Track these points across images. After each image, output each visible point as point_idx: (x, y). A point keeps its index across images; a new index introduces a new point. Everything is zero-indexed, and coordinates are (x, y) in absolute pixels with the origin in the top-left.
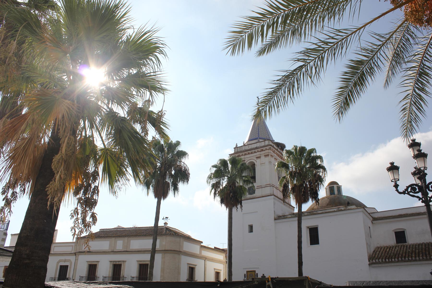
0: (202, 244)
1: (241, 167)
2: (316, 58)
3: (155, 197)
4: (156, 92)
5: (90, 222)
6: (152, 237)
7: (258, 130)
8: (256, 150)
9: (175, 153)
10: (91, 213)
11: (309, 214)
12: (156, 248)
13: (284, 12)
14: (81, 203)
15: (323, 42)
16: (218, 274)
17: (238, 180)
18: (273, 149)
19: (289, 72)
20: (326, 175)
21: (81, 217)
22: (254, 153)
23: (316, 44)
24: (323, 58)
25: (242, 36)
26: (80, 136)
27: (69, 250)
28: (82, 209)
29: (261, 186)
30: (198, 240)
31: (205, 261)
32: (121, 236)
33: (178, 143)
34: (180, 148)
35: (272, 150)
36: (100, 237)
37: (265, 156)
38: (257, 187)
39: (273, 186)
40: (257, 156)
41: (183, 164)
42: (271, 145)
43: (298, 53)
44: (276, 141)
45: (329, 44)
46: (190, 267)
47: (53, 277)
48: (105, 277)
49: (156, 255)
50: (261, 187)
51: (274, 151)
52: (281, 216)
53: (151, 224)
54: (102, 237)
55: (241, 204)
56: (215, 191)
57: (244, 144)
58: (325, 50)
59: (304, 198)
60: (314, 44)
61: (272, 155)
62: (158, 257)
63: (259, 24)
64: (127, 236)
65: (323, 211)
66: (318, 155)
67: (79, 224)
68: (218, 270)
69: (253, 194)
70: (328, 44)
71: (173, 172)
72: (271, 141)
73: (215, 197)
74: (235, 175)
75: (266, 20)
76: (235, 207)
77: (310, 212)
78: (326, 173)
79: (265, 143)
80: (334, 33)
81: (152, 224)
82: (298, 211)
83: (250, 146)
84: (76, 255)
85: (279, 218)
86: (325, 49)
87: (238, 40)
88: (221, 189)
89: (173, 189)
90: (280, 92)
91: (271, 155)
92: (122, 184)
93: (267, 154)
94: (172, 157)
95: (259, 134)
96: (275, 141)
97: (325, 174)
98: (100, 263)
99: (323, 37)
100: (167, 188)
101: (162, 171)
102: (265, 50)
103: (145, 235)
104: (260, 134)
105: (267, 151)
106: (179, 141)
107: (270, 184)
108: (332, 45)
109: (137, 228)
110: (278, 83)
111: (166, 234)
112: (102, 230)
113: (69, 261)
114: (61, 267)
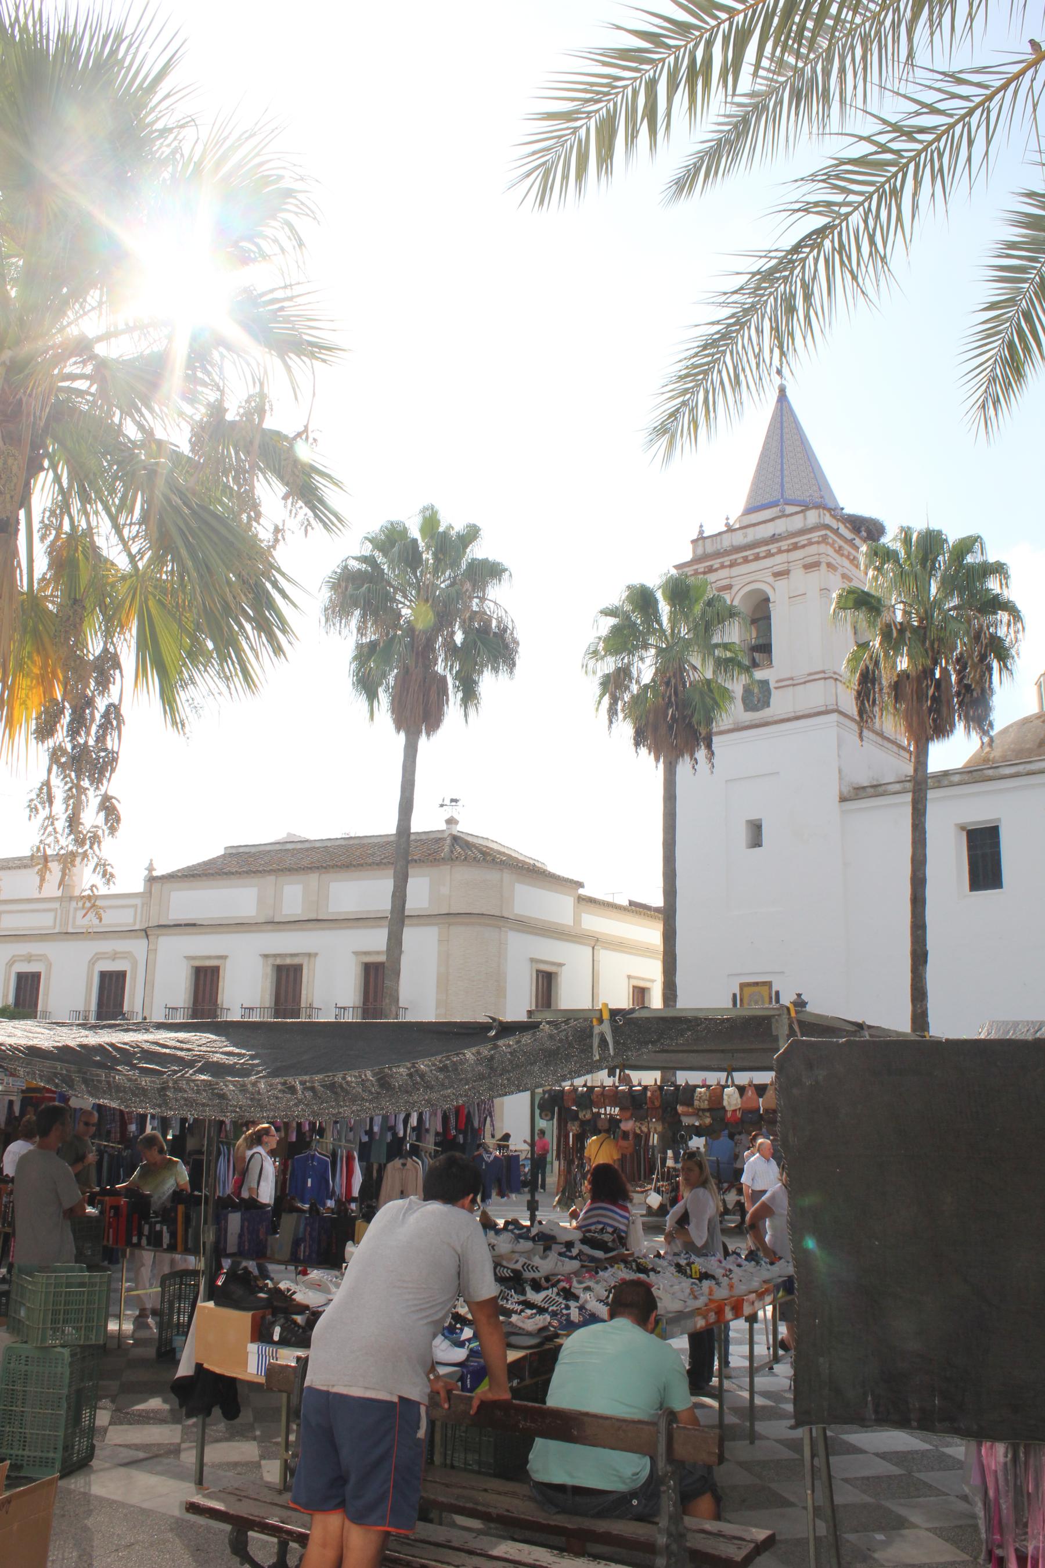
0: (581, 891)
1: (704, 613)
2: (871, 194)
3: (398, 729)
4: (303, 357)
5: (97, 827)
6: (392, 872)
7: (782, 470)
8: (773, 548)
9: (464, 566)
10: (100, 797)
11: (966, 777)
12: (407, 906)
13: (730, 19)
14: (62, 766)
15: (896, 128)
16: (640, 993)
17: (696, 660)
18: (834, 541)
19: (775, 258)
20: (1020, 636)
21: (66, 810)
22: (765, 557)
23: (868, 139)
24: (896, 194)
25: (576, 130)
26: (54, 532)
27: (125, 919)
28: (66, 783)
29: (792, 679)
30: (566, 876)
31: (593, 948)
32: (296, 870)
33: (472, 534)
34: (478, 551)
35: (832, 545)
36: (226, 874)
37: (808, 567)
38: (777, 682)
39: (836, 679)
40: (777, 569)
41: (492, 605)
42: (827, 527)
43: (802, 179)
44: (849, 510)
45: (919, 136)
46: (538, 972)
47: (81, 1007)
48: (250, 1009)
49: (406, 930)
50: (790, 682)
51: (840, 547)
52: (864, 788)
53: (388, 826)
54: (233, 873)
55: (709, 746)
56: (614, 701)
57: (727, 525)
58: (904, 161)
59: (934, 720)
60: (861, 138)
61: (834, 562)
62: (410, 935)
63: (639, 75)
64: (318, 868)
65: (1020, 768)
66: (991, 559)
67: (58, 835)
68: (643, 979)
69: (762, 708)
70: (915, 135)
71: (459, 638)
72: (829, 510)
73: (611, 722)
74: (681, 643)
75: (663, 60)
76: (687, 758)
77: (971, 772)
78: (1019, 625)
79: (805, 518)
80: (939, 90)
81: (388, 826)
82: (916, 770)
83: (750, 530)
84: (147, 936)
85: (857, 795)
86: (903, 157)
87: (563, 145)
88: (635, 692)
89: (462, 699)
90: (743, 337)
91: (829, 565)
92: (205, 694)
93: (815, 559)
94: (452, 585)
95: (782, 486)
96: (846, 511)
97: (1016, 632)
98: (228, 961)
99: (895, 110)
100: (438, 694)
101: (418, 635)
102: (698, 170)
103: (377, 864)
104: (786, 486)
105: (813, 549)
106: (475, 526)
107: (824, 672)
108: (929, 137)
109: (351, 838)
110: (736, 303)
111: (451, 859)
112: (234, 851)
113: (41, 960)
114: (104, 976)
